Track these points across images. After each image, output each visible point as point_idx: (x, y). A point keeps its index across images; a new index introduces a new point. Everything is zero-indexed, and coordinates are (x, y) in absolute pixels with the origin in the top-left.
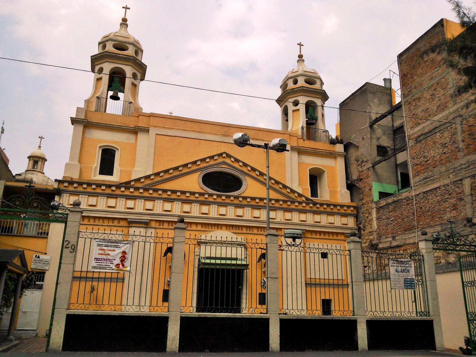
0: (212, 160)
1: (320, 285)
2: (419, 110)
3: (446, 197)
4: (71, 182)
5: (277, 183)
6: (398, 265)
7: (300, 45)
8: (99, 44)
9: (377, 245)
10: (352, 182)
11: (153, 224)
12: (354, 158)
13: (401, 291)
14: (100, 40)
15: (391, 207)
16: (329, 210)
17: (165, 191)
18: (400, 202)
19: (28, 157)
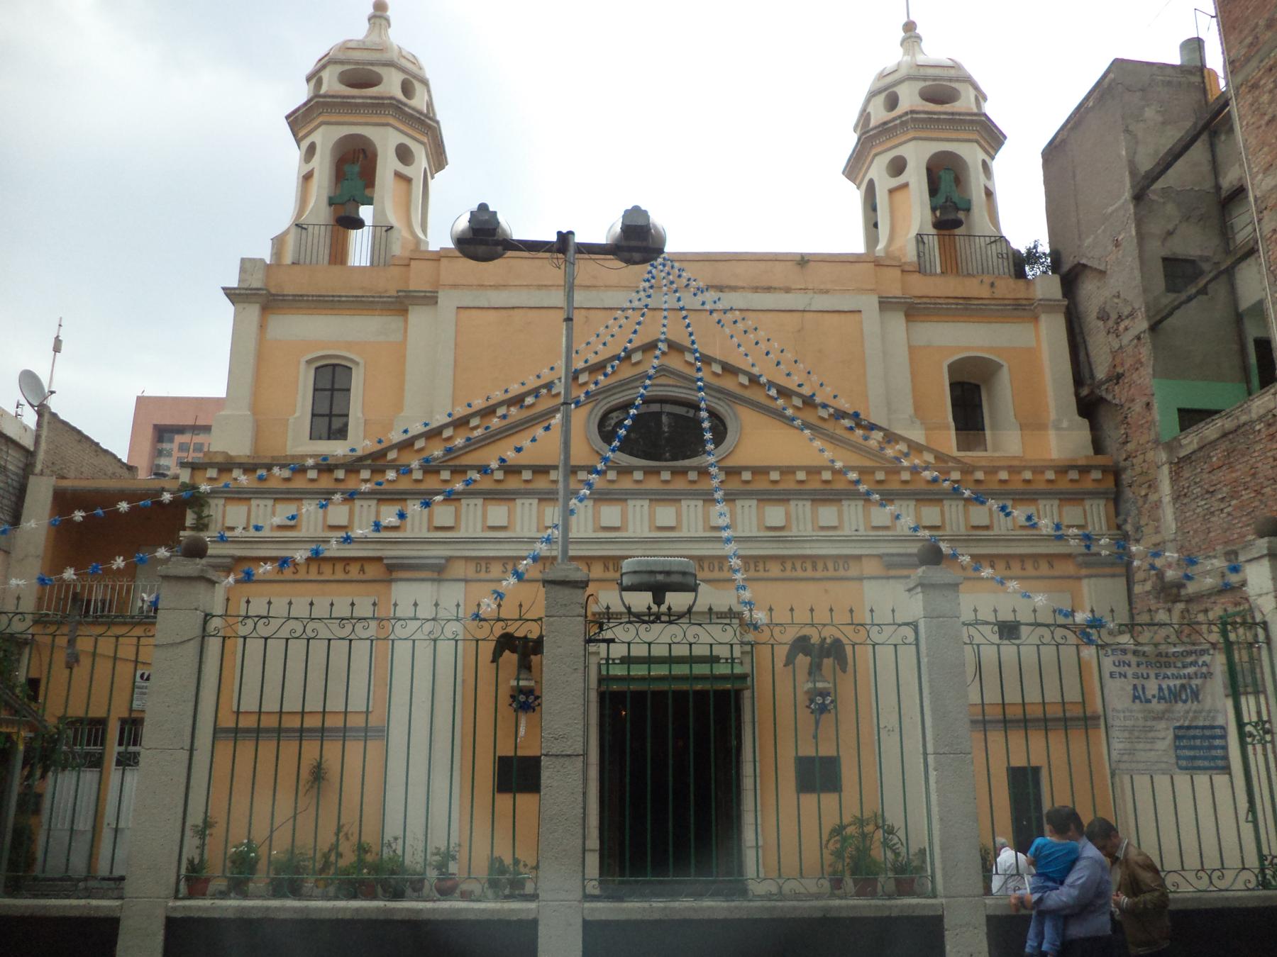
0: (626, 365)
6: (1143, 670)
10: (1092, 392)
12: (1094, 315)
13: (1162, 782)
15: (1216, 456)
18: (1245, 434)
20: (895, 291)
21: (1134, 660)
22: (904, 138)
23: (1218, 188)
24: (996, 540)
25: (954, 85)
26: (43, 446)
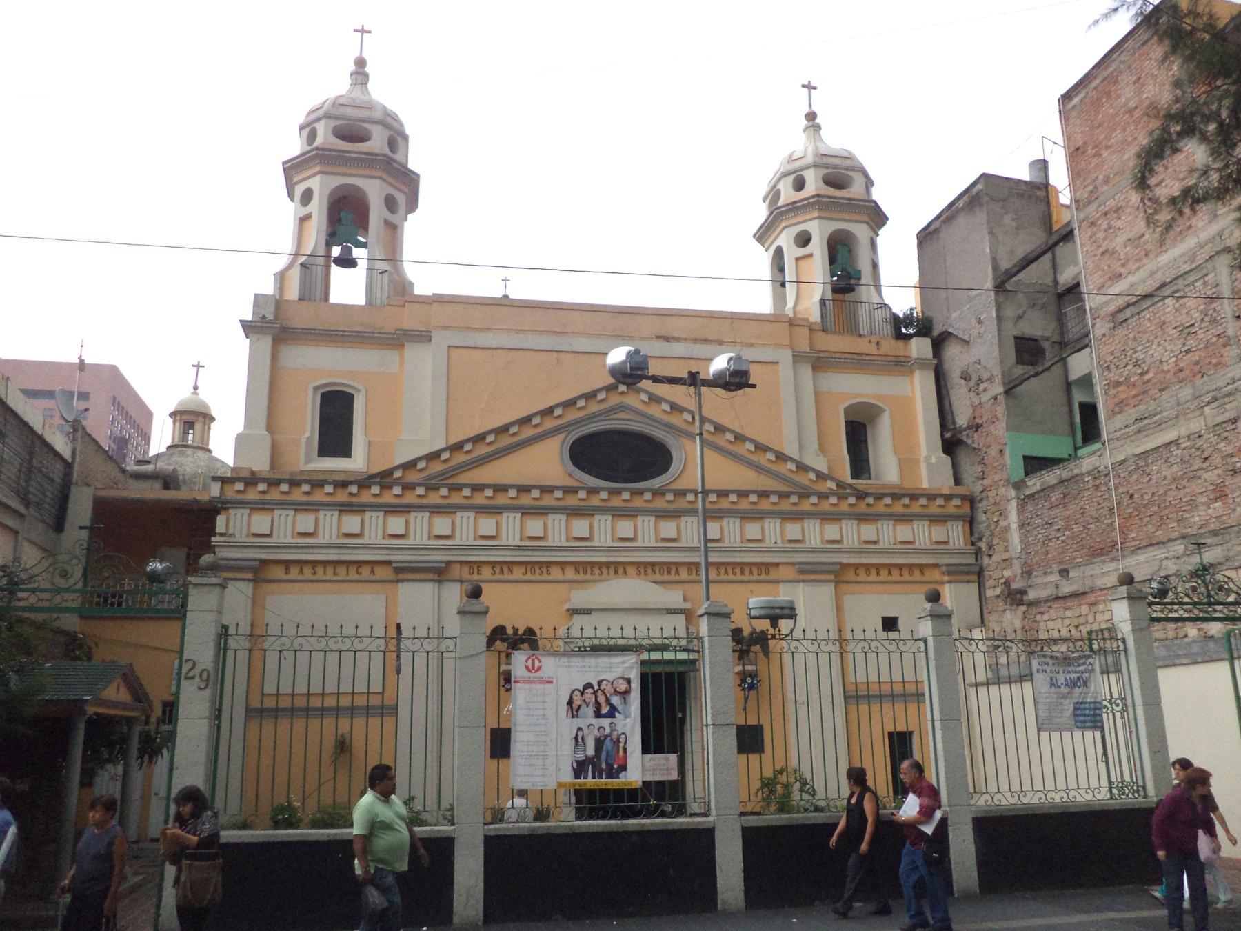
1: (880, 697)
2: (1120, 240)
3: (1196, 467)
4: (251, 480)
5: (761, 448)
7: (809, 87)
8: (302, 128)
9: (1023, 592)
10: (953, 436)
11: (456, 571)
14: (301, 119)
15: (1055, 496)
16: (898, 508)
17: (477, 488)
19: (171, 415)
20: (804, 346)
21: (1051, 662)
22: (808, 217)
23: (1056, 282)
24: (881, 552)
25: (850, 173)
26: (78, 459)
